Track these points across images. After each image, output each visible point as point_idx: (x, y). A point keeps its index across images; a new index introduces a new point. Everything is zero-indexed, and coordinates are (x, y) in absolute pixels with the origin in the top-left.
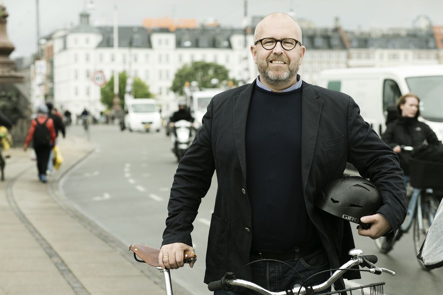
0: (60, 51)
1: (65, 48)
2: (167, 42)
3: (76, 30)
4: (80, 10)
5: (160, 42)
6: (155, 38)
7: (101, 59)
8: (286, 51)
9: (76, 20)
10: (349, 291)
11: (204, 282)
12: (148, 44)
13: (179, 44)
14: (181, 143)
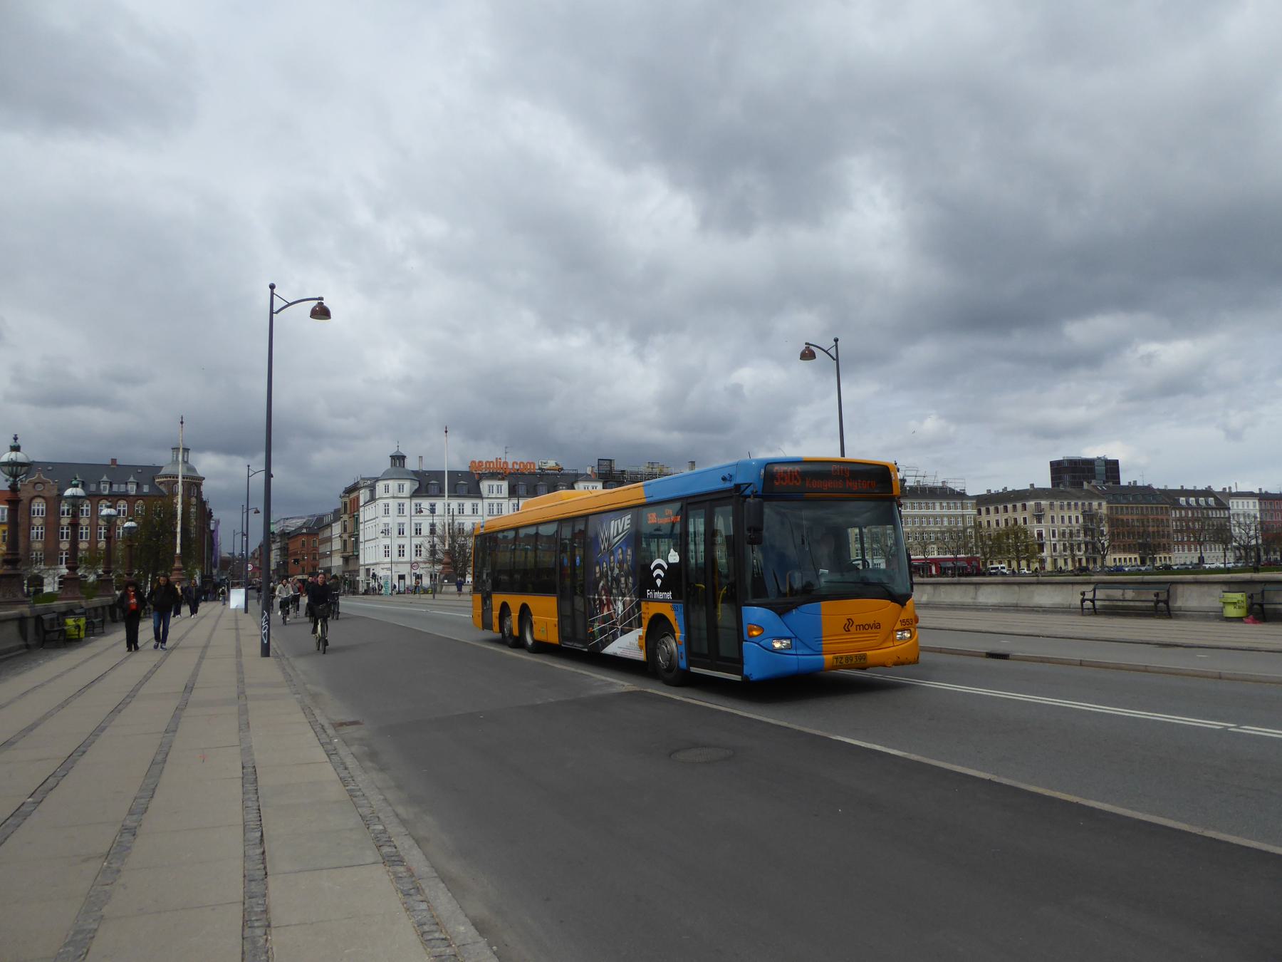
0: (395, 873)
1: (373, 499)
2: (499, 489)
3: (386, 476)
4: (393, 451)
5: (491, 489)
6: (485, 485)
7: (461, 511)
9: (387, 464)
11: (1116, 462)
12: (1058, 469)
13: (513, 492)
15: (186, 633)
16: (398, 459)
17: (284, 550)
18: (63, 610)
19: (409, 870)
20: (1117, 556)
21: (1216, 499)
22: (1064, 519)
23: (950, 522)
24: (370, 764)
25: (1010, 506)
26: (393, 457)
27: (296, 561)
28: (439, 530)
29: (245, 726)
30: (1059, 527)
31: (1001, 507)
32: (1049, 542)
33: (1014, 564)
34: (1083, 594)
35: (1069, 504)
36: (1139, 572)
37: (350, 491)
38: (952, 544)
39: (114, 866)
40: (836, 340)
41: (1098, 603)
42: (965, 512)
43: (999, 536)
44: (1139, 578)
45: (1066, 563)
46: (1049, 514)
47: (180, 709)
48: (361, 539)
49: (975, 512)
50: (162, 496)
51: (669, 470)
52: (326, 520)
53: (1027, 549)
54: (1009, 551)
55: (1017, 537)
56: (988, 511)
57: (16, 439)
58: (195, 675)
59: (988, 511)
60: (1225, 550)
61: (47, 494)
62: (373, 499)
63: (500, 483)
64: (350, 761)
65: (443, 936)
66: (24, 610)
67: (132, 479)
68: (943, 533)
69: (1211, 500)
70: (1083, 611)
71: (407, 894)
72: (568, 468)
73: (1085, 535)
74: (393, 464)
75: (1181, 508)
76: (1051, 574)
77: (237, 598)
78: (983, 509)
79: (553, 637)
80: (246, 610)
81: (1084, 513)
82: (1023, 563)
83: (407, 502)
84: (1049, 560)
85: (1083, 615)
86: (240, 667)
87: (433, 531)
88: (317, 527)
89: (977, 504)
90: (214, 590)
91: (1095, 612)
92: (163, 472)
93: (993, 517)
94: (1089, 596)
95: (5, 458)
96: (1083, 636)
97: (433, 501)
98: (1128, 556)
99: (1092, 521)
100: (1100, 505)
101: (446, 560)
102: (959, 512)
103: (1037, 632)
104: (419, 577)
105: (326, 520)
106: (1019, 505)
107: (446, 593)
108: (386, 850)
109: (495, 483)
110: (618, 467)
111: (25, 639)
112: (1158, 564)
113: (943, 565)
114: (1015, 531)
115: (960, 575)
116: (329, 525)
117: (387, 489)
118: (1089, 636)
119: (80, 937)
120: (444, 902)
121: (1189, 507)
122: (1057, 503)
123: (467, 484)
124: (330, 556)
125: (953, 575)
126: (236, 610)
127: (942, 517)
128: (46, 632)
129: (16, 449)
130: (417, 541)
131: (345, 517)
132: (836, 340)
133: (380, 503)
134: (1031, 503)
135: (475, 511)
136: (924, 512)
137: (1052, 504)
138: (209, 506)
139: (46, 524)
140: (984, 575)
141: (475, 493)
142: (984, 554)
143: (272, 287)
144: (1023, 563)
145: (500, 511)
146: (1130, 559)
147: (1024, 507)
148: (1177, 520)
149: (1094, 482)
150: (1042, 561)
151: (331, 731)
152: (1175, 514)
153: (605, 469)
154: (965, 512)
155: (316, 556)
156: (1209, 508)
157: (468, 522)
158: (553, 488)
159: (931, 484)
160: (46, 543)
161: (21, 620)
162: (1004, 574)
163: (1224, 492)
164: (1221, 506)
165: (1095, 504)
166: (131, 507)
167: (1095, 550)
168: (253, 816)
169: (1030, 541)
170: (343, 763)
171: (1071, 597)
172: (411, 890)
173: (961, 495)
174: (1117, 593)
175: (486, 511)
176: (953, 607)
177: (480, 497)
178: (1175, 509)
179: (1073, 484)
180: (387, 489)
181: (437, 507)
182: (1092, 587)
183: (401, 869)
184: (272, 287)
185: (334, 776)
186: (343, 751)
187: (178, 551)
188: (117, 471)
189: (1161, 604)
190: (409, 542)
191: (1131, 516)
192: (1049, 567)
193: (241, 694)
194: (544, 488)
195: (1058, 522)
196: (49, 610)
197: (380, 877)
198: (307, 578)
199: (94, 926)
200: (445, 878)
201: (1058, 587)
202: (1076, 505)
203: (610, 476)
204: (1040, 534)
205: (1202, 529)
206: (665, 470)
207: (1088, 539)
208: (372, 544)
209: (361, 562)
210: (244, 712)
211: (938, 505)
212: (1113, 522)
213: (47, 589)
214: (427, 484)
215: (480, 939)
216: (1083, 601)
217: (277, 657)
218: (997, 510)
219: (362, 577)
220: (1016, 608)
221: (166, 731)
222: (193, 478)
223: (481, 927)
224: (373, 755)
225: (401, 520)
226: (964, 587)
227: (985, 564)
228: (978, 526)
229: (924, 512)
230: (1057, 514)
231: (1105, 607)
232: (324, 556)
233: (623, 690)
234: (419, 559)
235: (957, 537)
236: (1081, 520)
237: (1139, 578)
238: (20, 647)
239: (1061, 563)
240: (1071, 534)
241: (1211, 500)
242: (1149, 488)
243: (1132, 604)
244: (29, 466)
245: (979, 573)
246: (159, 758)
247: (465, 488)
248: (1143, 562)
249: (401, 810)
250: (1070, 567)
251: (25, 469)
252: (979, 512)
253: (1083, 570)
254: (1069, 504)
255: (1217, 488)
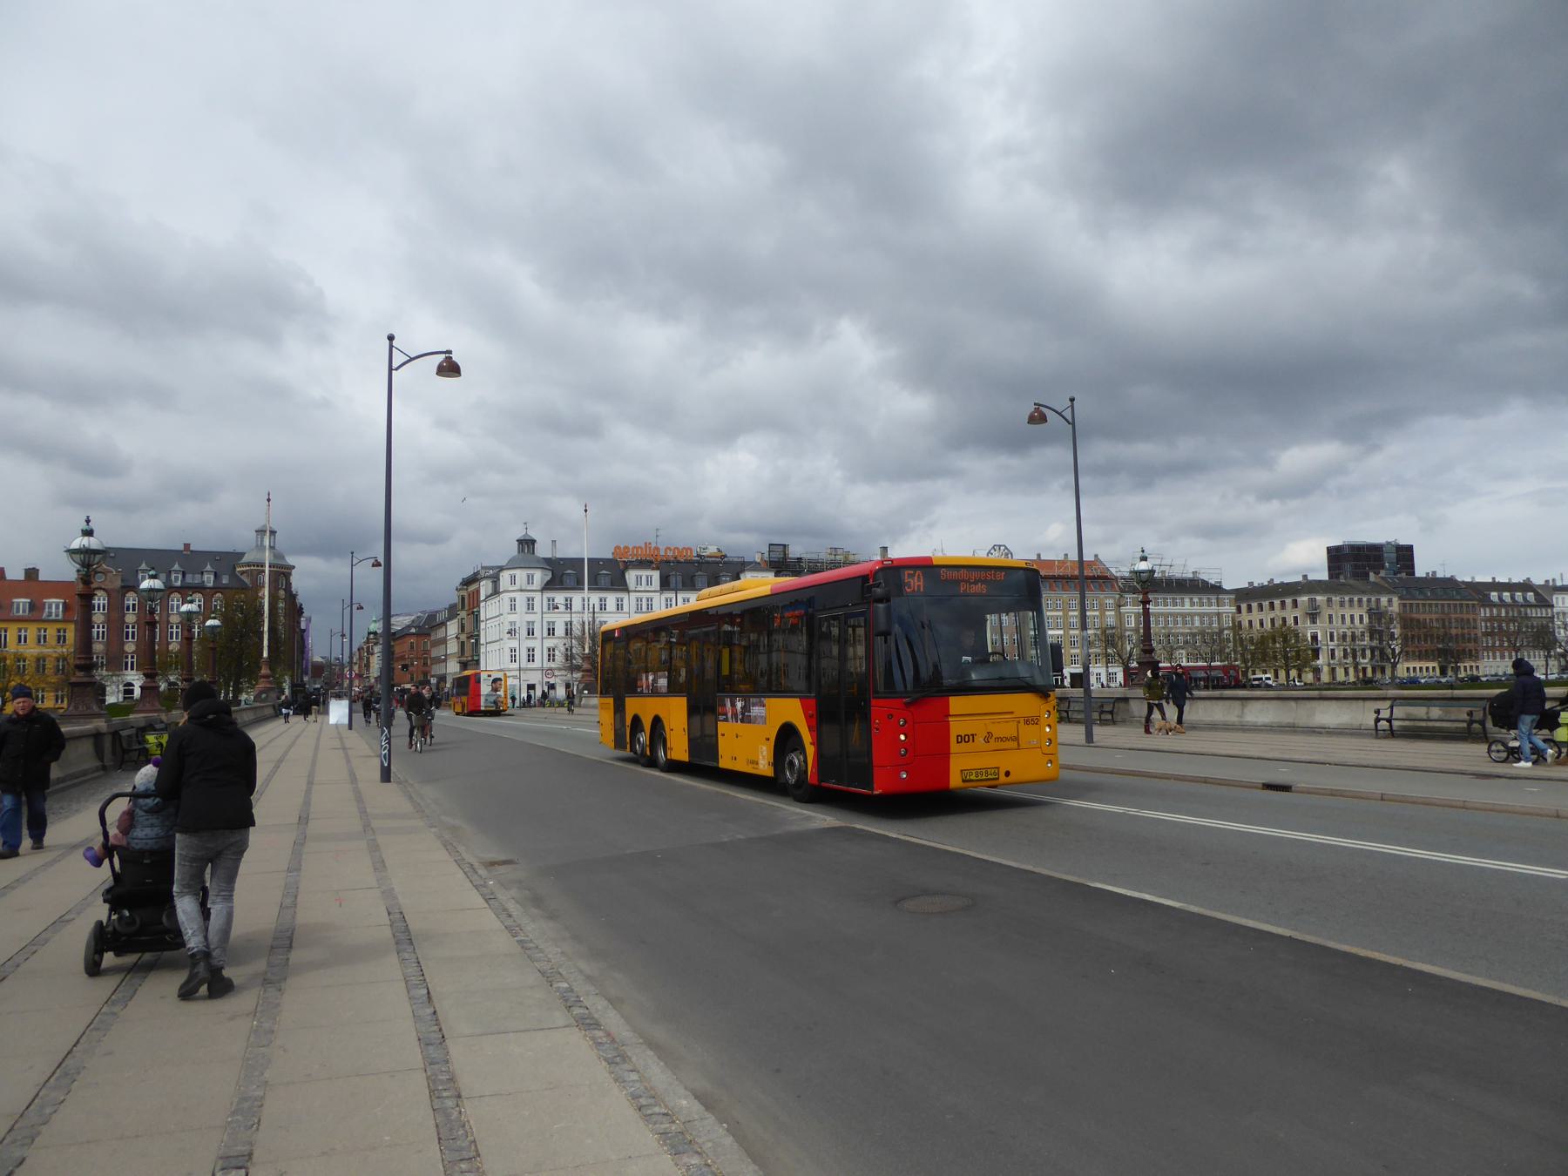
1: (496, 592)
2: (649, 581)
3: (512, 565)
4: (520, 535)
5: (638, 580)
6: (631, 576)
7: (603, 607)
8: (107, 795)
9: (513, 549)
10: (1072, 597)
11: (1410, 549)
12: (1336, 556)
13: (665, 585)
14: (96, 1026)
15: (286, 753)
16: (527, 544)
17: (389, 656)
18: (142, 724)
19: (608, 1035)
20: (1411, 665)
21: (1537, 594)
22: (1339, 622)
23: (1202, 622)
24: (535, 911)
25: (1277, 603)
26: (520, 542)
27: (405, 667)
28: (577, 631)
29: (380, 866)
30: (1339, 628)
31: (1266, 604)
32: (1325, 646)
33: (1282, 674)
34: (1378, 712)
35: (1351, 601)
36: (1438, 685)
37: (468, 582)
38: (1205, 649)
39: (266, 1025)
40: (1072, 400)
41: (1396, 724)
42: (1222, 609)
43: (1263, 640)
44: (1448, 693)
45: (1347, 673)
46: (1326, 612)
47: (299, 845)
48: (482, 641)
49: (1234, 609)
50: (244, 588)
51: (857, 558)
52: (440, 618)
53: (1298, 657)
54: (1275, 658)
55: (1285, 640)
56: (1250, 609)
57: (88, 521)
58: (307, 803)
59: (1250, 609)
60: (1547, 657)
61: (109, 587)
62: (496, 592)
63: (649, 572)
64: (512, 907)
65: (664, 1111)
66: (100, 724)
67: (209, 568)
68: (1193, 635)
69: (1530, 595)
70: (1377, 733)
71: (611, 1062)
72: (732, 555)
73: (1371, 639)
74: (521, 550)
75: (1492, 605)
76: (1328, 687)
77: (338, 711)
78: (1244, 607)
79: (685, 757)
80: (350, 726)
81: (1369, 611)
82: (1293, 673)
83: (537, 596)
84: (1326, 669)
85: (1377, 737)
86: (359, 798)
87: (568, 632)
88: (429, 626)
89: (1237, 600)
90: (307, 703)
91: (1392, 734)
92: (245, 559)
93: (1256, 616)
94: (1385, 714)
95: (76, 545)
96: (1379, 763)
97: (569, 594)
98: (1424, 665)
99: (1379, 620)
100: (1390, 601)
101: (586, 666)
102: (1214, 609)
103: (1321, 758)
104: (552, 687)
105: (440, 618)
106: (1288, 601)
107: (586, 707)
108: (577, 1011)
109: (644, 573)
110: (795, 551)
111: (101, 759)
112: (1462, 675)
113: (1193, 674)
114: (1284, 634)
115: (1214, 688)
116: (443, 624)
117: (513, 580)
118: (1371, 763)
119: (246, 1105)
120: (658, 1074)
121: (1502, 604)
122: (1336, 599)
123: (610, 574)
124: (445, 661)
125: (1206, 688)
126: (336, 726)
127: (1192, 615)
128: (125, 752)
129: (88, 533)
130: (550, 643)
131: (463, 614)
132: (1072, 400)
133: (506, 597)
134: (1303, 599)
135: (619, 607)
136: (1170, 609)
137: (1329, 600)
138: (300, 600)
139: (109, 620)
140: (1244, 687)
141: (619, 584)
142: (1245, 661)
143: (391, 338)
144: (1293, 673)
145: (650, 607)
146: (1427, 669)
147: (1295, 604)
148: (1486, 620)
149: (1383, 573)
150: (1317, 671)
151: (482, 872)
152: (1484, 613)
153: (777, 555)
154: (1222, 609)
155: (427, 661)
156: (1528, 605)
157: (614, 620)
158: (714, 581)
159: (1178, 575)
160: (108, 644)
161: (97, 736)
162: (1269, 687)
163: (1546, 586)
164: (1544, 603)
165: (1384, 600)
166: (207, 601)
167: (1383, 657)
168: (412, 970)
169: (1302, 645)
170: (505, 910)
171: (1363, 715)
172: (616, 1058)
173: (1216, 589)
174: (1420, 711)
175: (633, 608)
176: (1213, 727)
177: (626, 589)
178: (1484, 606)
179: (1355, 575)
180: (513, 580)
181: (625, 602)
182: (1388, 703)
183: (598, 1033)
184: (391, 338)
185: (497, 925)
186: (503, 896)
187: (265, 654)
188: (189, 558)
189: (1476, 726)
190: (540, 645)
191: (1429, 614)
192: (1325, 678)
193: (367, 826)
194: (705, 579)
195: (1337, 622)
196: (126, 726)
197: (576, 1040)
198: (414, 682)
199: (259, 1093)
200: (652, 1045)
201: (1346, 703)
202: (1360, 601)
203: (780, 564)
204: (1314, 638)
205: (1519, 632)
206: (851, 558)
207: (1375, 643)
208: (495, 646)
209: (482, 667)
210: (374, 848)
211: (1187, 601)
212: (1407, 623)
213: (111, 699)
214: (562, 575)
215: (707, 1115)
216: (1377, 720)
217: (399, 783)
218: (1261, 607)
219: (485, 689)
220: (1293, 729)
221: (289, 870)
222: (282, 567)
223: (707, 1102)
224: (537, 901)
225: (530, 618)
226: (1228, 703)
227: (1245, 673)
228: (1237, 626)
229: (1170, 609)
230: (1336, 612)
231: (1405, 728)
232: (438, 660)
233: (825, 825)
234: (553, 665)
235: (1212, 641)
236: (1366, 620)
237: (1448, 693)
238: (97, 769)
239: (1340, 676)
240: (1354, 637)
241: (1530, 595)
242: (1452, 580)
243: (1438, 724)
244: (103, 553)
245: (1239, 685)
246: (288, 901)
247: (608, 579)
248: (1443, 672)
249: (582, 965)
250: (1352, 679)
251: (98, 557)
252: (1239, 610)
253: (1367, 683)
254: (1351, 601)
255: (1538, 580)
